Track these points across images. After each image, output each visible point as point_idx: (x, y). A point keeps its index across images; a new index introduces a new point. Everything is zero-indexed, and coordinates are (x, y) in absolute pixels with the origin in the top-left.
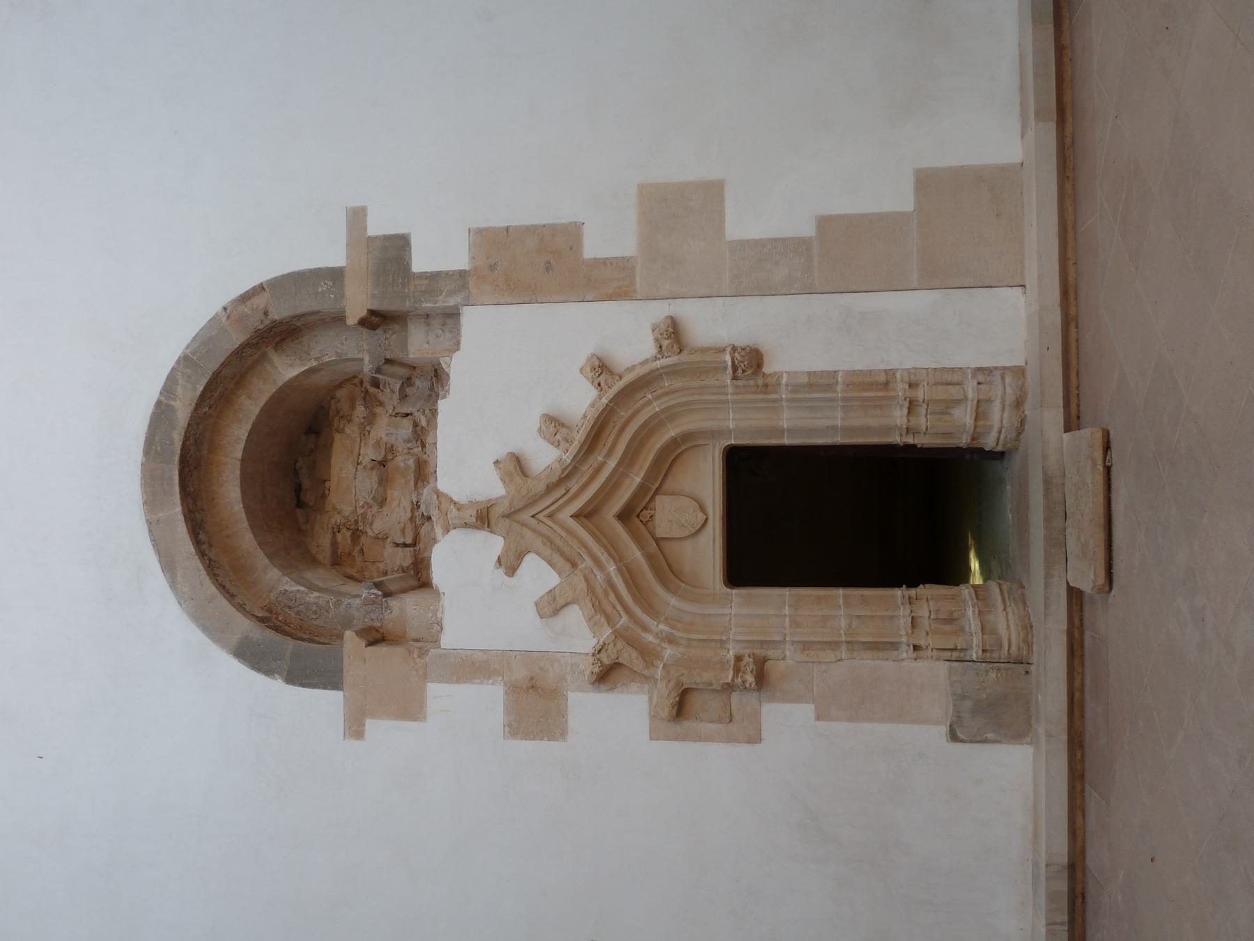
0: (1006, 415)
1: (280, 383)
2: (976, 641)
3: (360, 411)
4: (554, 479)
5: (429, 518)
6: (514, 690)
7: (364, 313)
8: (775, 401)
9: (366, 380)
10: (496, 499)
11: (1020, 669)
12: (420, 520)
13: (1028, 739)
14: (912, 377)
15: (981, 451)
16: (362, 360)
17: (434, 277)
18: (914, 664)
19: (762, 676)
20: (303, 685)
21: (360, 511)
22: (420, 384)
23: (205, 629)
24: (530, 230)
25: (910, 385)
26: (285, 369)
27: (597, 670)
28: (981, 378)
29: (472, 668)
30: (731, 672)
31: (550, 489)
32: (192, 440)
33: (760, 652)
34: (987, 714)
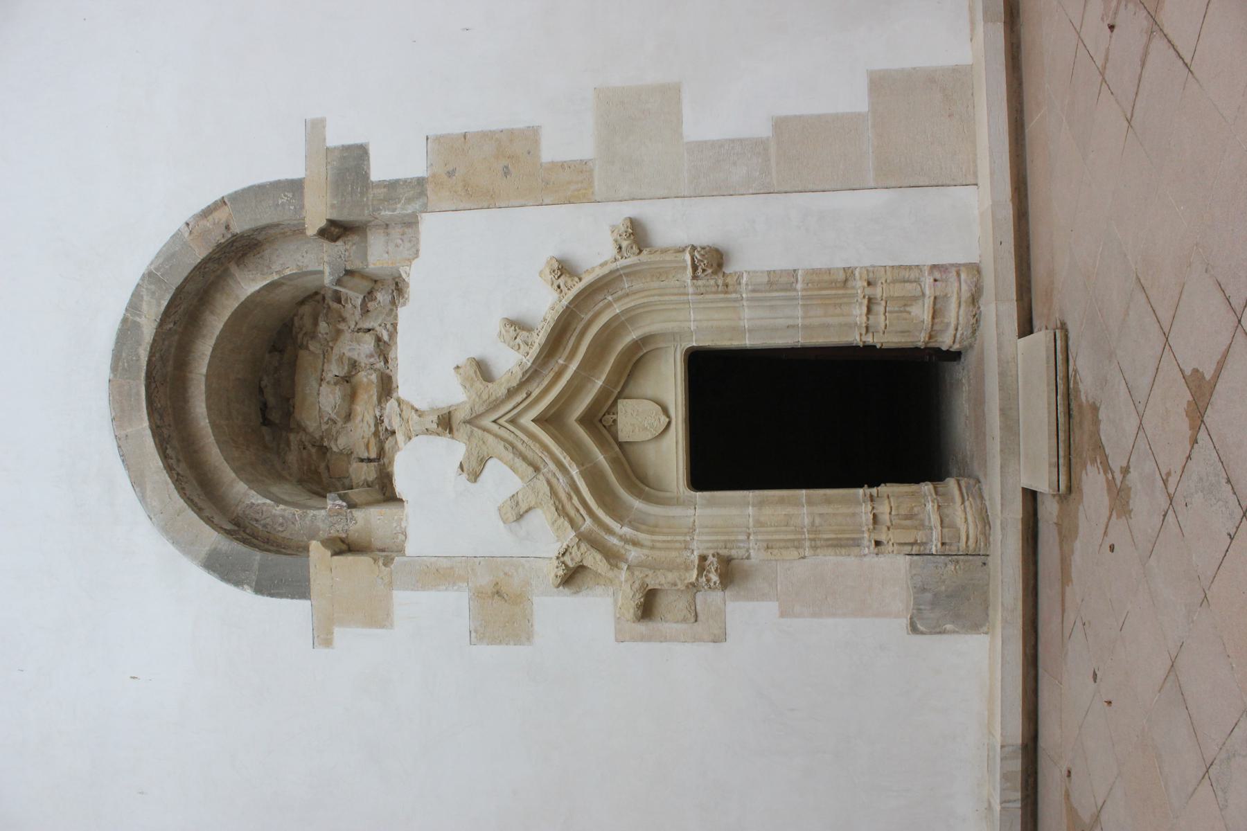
0: (961, 312)
1: (243, 298)
2: (936, 534)
3: (323, 326)
4: (515, 384)
5: (393, 433)
6: (477, 594)
7: (323, 223)
8: (735, 300)
9: (329, 295)
10: (458, 405)
11: (979, 560)
12: (383, 435)
13: (985, 629)
14: (871, 275)
15: (938, 351)
16: (322, 272)
17: (393, 185)
18: (876, 559)
19: (729, 572)
20: (272, 595)
21: (324, 427)
22: (382, 297)
23: (175, 542)
24: (486, 135)
25: (869, 284)
26: (248, 284)
27: (561, 573)
28: (937, 275)
29: (437, 574)
30: (695, 572)
31: (511, 393)
32: (157, 355)
33: (723, 552)
34: (945, 605)
